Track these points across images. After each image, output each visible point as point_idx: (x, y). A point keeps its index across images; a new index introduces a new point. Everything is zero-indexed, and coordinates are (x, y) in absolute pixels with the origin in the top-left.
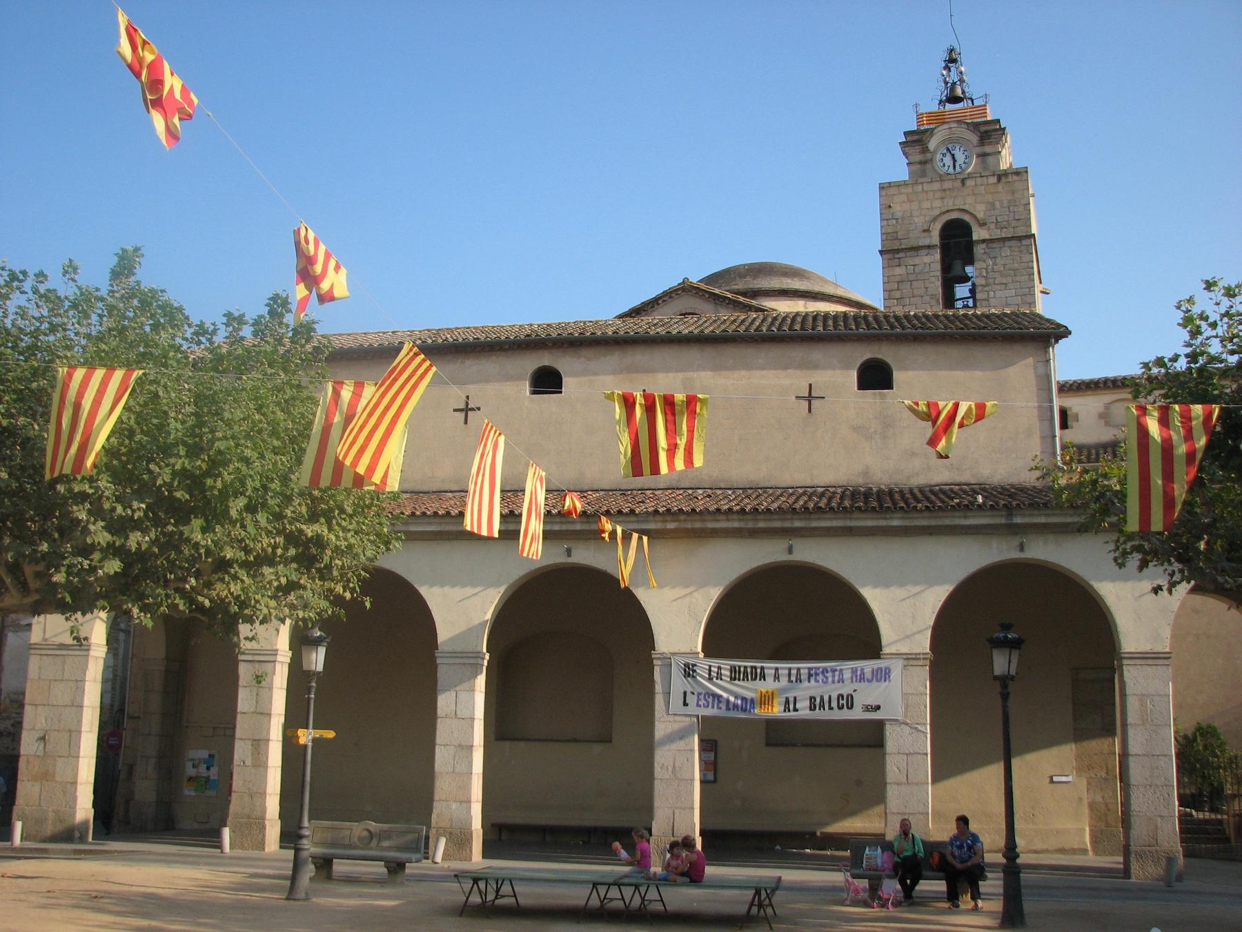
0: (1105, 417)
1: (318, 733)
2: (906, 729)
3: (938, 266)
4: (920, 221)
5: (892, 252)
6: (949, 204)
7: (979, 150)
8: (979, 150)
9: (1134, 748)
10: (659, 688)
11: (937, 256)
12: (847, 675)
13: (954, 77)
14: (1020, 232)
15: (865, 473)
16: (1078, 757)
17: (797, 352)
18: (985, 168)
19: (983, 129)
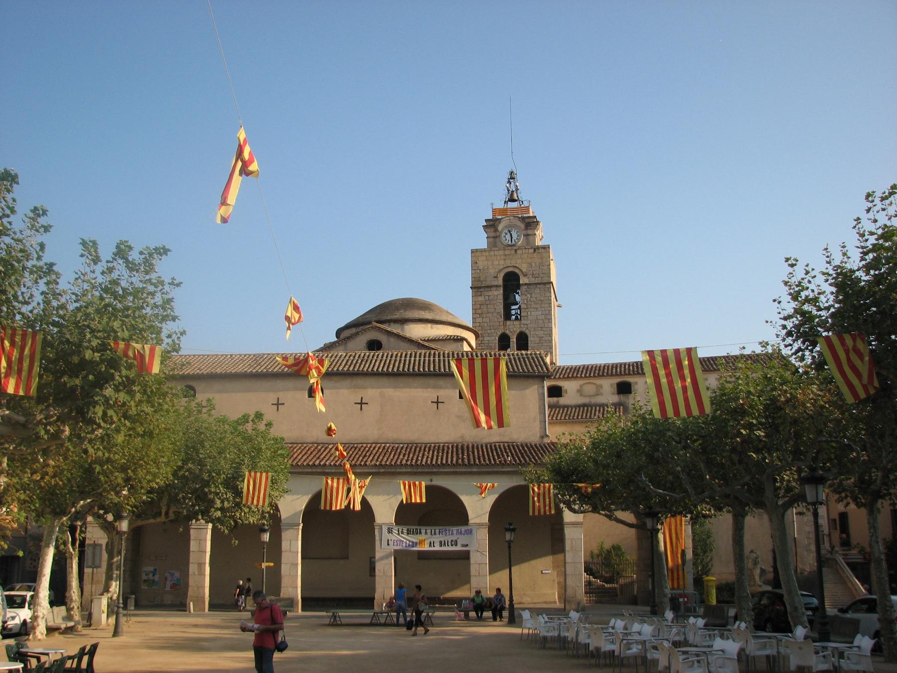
0: (580, 391)
1: (267, 564)
2: (479, 554)
3: (501, 297)
4: (492, 272)
5: (477, 288)
6: (508, 263)
7: (525, 232)
8: (525, 232)
9: (568, 560)
10: (377, 538)
11: (501, 291)
12: (455, 532)
13: (513, 188)
14: (545, 280)
15: (462, 437)
16: (553, 562)
17: (432, 381)
18: (528, 243)
19: (527, 220)
